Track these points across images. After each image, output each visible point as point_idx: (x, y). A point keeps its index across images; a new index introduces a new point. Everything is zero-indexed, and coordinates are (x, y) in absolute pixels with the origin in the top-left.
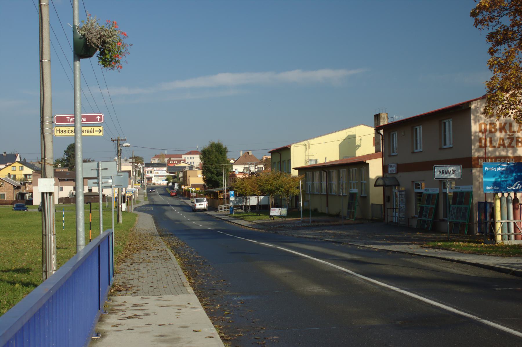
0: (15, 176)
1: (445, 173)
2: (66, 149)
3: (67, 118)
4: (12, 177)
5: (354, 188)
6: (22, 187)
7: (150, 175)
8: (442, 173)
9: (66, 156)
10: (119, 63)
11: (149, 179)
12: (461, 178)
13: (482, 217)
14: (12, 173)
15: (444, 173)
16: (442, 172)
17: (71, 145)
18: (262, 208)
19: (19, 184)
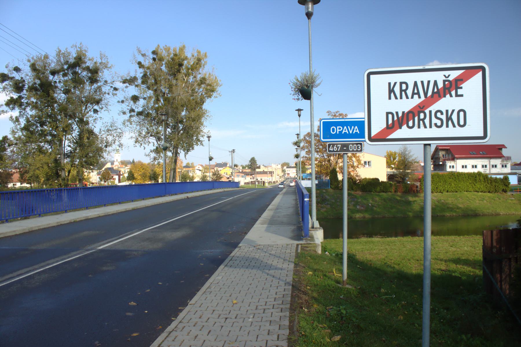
0: (227, 173)
1: (413, 94)
2: (250, 160)
3: (354, 133)
4: (226, 173)
5: (309, 190)
6: (230, 178)
7: (289, 172)
8: (398, 95)
9: (250, 163)
10: (56, 157)
11: (288, 174)
12: (483, 69)
13: (13, 207)
14: (226, 172)
15: (409, 92)
16: (401, 90)
17: (252, 158)
18: (358, 216)
19: (228, 176)
